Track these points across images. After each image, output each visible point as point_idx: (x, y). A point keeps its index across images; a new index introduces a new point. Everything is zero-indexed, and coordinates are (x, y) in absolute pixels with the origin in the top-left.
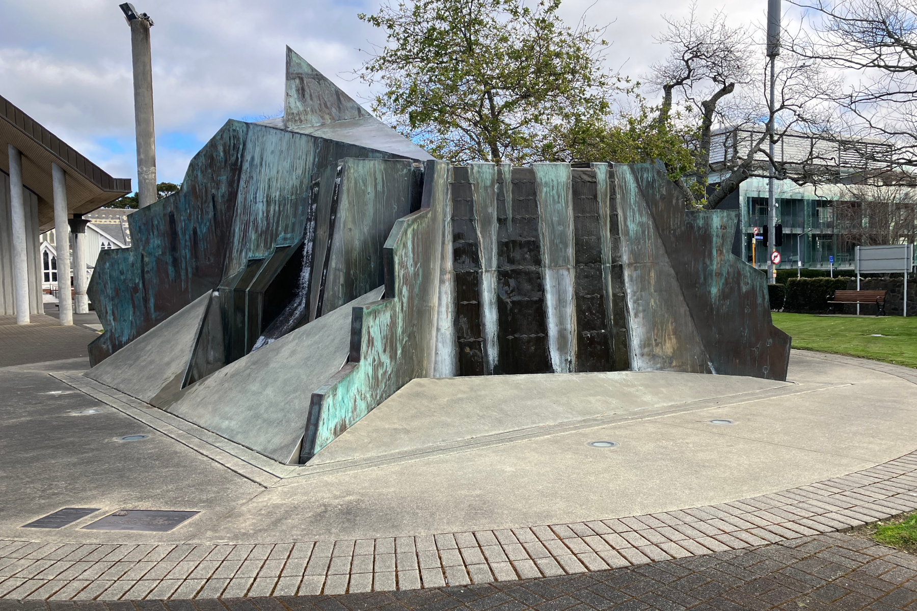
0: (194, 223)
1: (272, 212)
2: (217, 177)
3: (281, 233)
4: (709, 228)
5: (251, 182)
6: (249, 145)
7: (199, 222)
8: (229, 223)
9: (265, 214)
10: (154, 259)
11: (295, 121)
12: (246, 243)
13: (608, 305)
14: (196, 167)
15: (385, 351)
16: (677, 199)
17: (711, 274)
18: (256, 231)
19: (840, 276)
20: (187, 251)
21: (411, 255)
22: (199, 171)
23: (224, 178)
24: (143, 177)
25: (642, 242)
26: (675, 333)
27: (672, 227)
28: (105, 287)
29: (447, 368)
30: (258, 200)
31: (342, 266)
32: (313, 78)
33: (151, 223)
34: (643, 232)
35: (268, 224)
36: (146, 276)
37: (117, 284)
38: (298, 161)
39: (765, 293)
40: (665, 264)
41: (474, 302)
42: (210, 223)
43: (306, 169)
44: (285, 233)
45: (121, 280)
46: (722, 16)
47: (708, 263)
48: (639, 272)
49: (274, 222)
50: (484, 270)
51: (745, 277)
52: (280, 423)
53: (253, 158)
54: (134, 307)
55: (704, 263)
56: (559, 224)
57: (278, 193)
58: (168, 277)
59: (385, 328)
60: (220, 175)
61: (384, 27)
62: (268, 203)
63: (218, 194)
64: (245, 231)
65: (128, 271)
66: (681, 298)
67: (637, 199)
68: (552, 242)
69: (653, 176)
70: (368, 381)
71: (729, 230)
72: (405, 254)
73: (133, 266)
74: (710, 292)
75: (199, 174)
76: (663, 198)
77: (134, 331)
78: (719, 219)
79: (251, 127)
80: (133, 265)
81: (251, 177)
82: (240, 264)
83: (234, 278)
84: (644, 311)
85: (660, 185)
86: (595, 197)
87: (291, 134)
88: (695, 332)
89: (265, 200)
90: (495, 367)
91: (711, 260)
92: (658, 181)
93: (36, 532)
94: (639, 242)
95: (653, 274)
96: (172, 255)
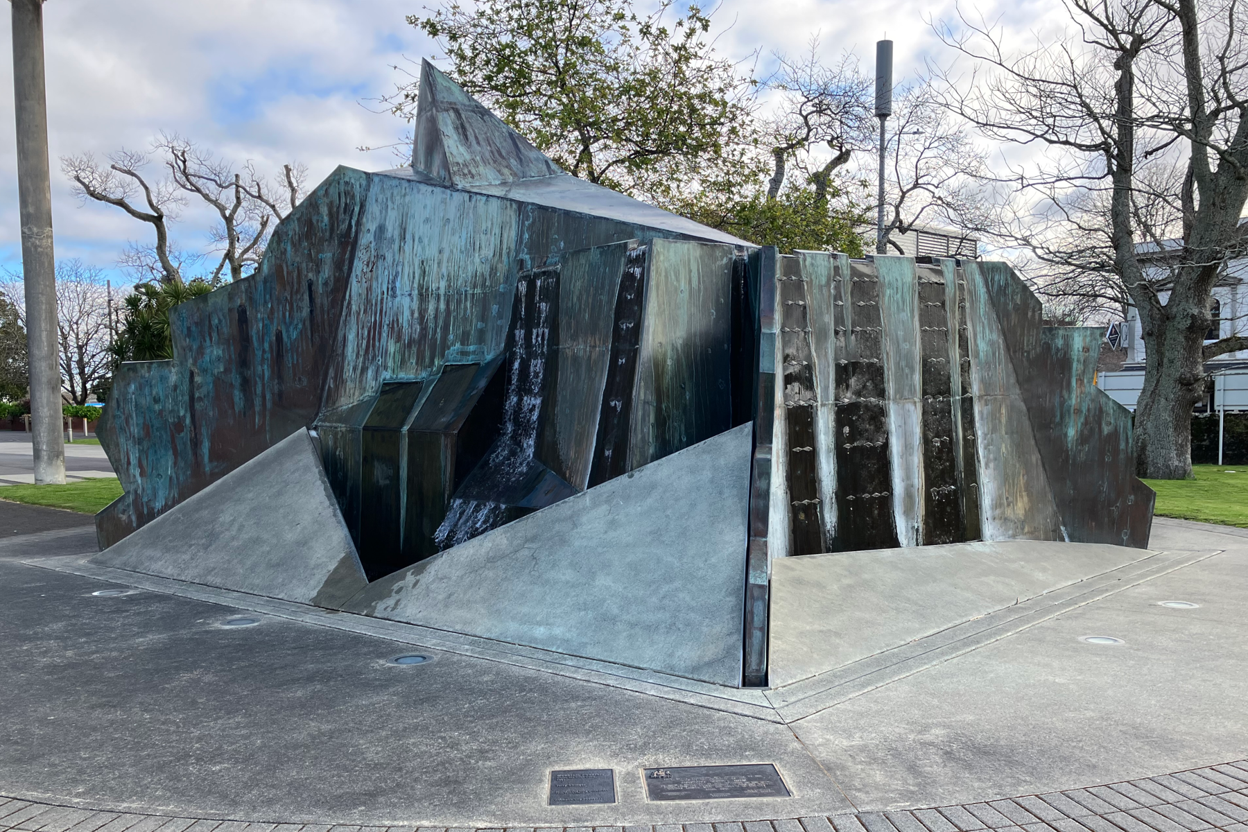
0: (278, 324)
2: (318, 253)
6: (373, 209)
7: (285, 323)
9: (416, 315)
10: (210, 379)
11: (465, 175)
12: (374, 357)
13: (958, 452)
17: (1069, 411)
18: (399, 339)
20: (266, 367)
22: (289, 244)
23: (327, 256)
24: (33, 244)
25: (992, 366)
26: (1027, 490)
27: (1026, 348)
28: (127, 422)
29: (779, 542)
30: (398, 292)
31: (651, 398)
32: (474, 112)
33: (207, 323)
34: (994, 354)
35: (424, 329)
36: (197, 406)
37: (147, 417)
38: (483, 237)
40: (1016, 394)
41: (808, 449)
42: (304, 324)
43: (501, 249)
45: (155, 412)
46: (853, 58)
47: (1066, 397)
48: (989, 407)
50: (819, 404)
51: (1108, 414)
52: (674, 628)
53: (381, 229)
54: (175, 453)
55: (1061, 396)
56: (905, 341)
57: (443, 284)
58: (233, 408)
60: (321, 251)
61: (444, 38)
62: (423, 295)
63: (318, 280)
65: (167, 397)
66: (1033, 442)
68: (897, 364)
71: (1092, 353)
74: (1066, 435)
75: (289, 248)
76: (1016, 308)
77: (175, 493)
78: (1081, 338)
79: (376, 179)
80: (175, 388)
84: (995, 459)
85: (1013, 291)
86: (943, 304)
87: (467, 196)
88: (1047, 489)
89: (415, 292)
90: (835, 540)
91: (1070, 392)
93: (600, 810)
94: (990, 367)
95: (1003, 411)
96: (241, 374)
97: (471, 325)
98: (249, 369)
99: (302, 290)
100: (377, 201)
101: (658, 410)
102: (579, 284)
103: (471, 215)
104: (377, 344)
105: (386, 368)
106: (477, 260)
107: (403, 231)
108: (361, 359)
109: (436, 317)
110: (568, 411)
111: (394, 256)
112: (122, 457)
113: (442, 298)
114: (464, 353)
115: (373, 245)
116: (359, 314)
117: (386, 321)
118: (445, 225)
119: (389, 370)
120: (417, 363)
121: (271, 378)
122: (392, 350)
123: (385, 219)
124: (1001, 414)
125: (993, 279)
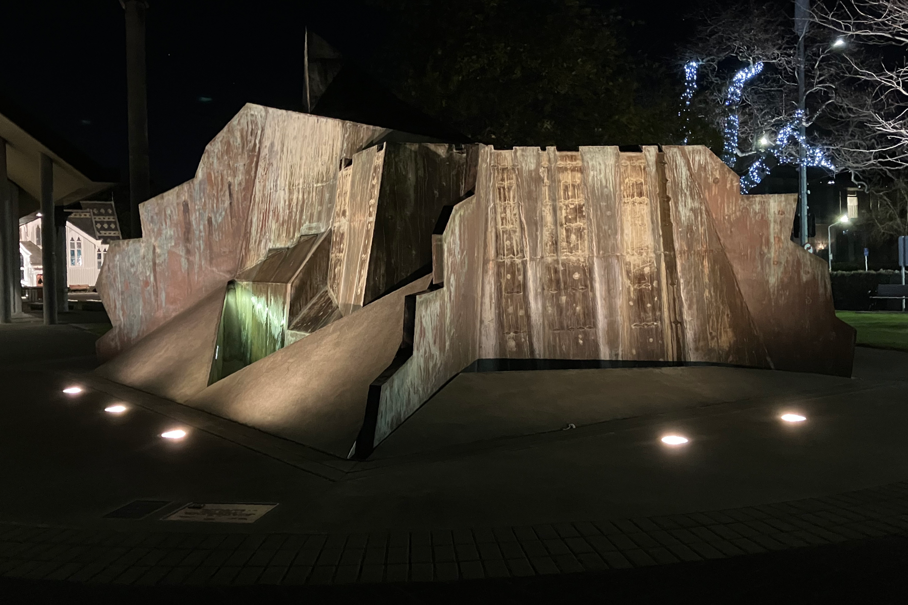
0: (209, 213)
1: (295, 201)
2: (234, 163)
3: (305, 222)
4: (766, 213)
5: (270, 169)
6: (268, 131)
7: (214, 212)
8: (247, 211)
9: (287, 203)
12: (265, 233)
14: (212, 154)
15: (435, 343)
16: (732, 183)
19: (881, 269)
20: (201, 242)
21: (459, 242)
22: (215, 158)
23: (241, 164)
30: (278, 188)
33: (163, 213)
34: (696, 218)
35: (290, 213)
36: (158, 269)
38: (323, 146)
39: (827, 283)
44: (310, 222)
45: (131, 273)
47: (766, 251)
49: (297, 211)
51: (805, 265)
53: (272, 145)
57: (301, 181)
59: (435, 318)
64: (265, 220)
65: (138, 263)
67: (689, 183)
69: (706, 159)
70: (420, 373)
72: (453, 240)
73: (144, 258)
74: (768, 282)
75: (215, 161)
76: (716, 181)
81: (271, 164)
82: (259, 256)
83: (252, 270)
85: (713, 168)
91: (769, 249)
92: (711, 163)
95: (706, 263)
96: (186, 247)
97: (315, 209)
98: (190, 243)
99: (224, 189)
101: (388, 265)
108: (259, 235)
112: (111, 303)
114: (310, 228)
115: (267, 156)
119: (272, 242)
120: (286, 237)
122: (274, 227)
124: (703, 266)
125: (694, 159)
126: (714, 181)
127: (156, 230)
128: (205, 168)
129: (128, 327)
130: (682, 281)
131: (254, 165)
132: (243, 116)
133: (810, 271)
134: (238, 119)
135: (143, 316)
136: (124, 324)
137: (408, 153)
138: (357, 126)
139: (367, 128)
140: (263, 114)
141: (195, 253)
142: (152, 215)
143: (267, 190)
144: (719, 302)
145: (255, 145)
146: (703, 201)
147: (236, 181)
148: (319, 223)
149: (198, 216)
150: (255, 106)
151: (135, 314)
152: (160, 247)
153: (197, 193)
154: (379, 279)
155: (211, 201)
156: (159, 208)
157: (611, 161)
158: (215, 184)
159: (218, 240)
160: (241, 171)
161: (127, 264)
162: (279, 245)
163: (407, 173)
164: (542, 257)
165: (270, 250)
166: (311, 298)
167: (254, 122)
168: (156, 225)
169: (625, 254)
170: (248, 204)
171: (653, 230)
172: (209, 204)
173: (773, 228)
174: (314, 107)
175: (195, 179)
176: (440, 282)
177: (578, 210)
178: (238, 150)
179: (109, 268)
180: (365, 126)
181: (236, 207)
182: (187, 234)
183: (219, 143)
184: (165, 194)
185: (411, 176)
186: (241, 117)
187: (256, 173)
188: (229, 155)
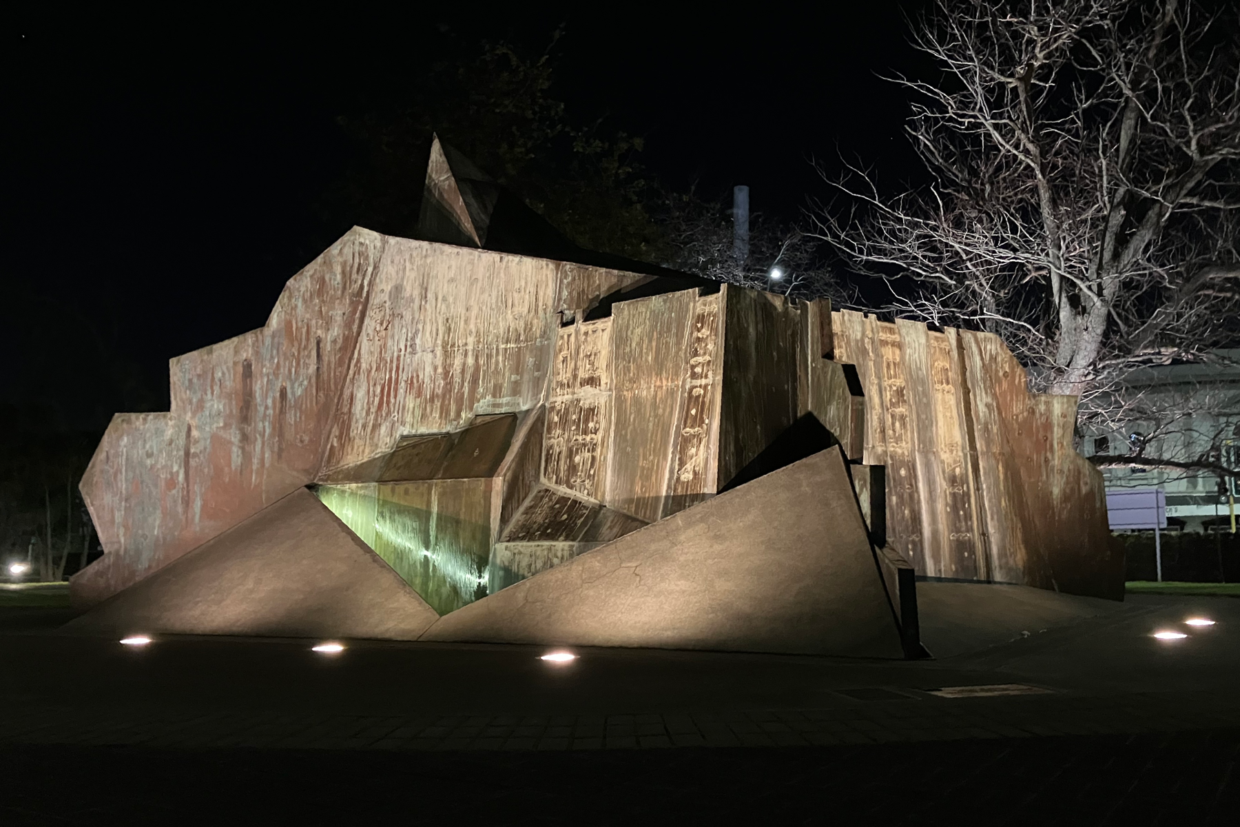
9: (440, 370)
14: (297, 293)
18: (419, 394)
20: (267, 424)
22: (300, 300)
23: (338, 313)
27: (1015, 412)
33: (210, 375)
35: (449, 385)
36: (193, 462)
37: (138, 472)
38: (516, 295)
42: (310, 380)
43: (537, 306)
45: (146, 467)
47: (1050, 458)
49: (463, 382)
51: (1085, 475)
53: (398, 289)
57: (471, 340)
60: (333, 308)
65: (161, 451)
71: (1069, 419)
74: (1051, 492)
75: (300, 304)
78: (1060, 405)
85: (1003, 360)
97: (504, 378)
98: (250, 425)
99: (310, 347)
100: (392, 262)
102: (638, 331)
103: (502, 275)
104: (392, 400)
105: (403, 423)
106: (510, 317)
107: (425, 290)
108: (372, 417)
109: (463, 371)
110: (629, 449)
111: (413, 314)
113: (470, 353)
116: (369, 372)
117: (403, 377)
118: (472, 284)
119: (408, 426)
120: (441, 417)
121: (272, 436)
122: (411, 406)
123: (403, 279)
125: (985, 348)
126: (1004, 375)
127: (194, 400)
128: (283, 313)
129: (132, 553)
130: (984, 486)
131: (358, 315)
132: (348, 244)
133: (1089, 481)
134: (339, 248)
135: (161, 535)
136: (125, 549)
137: (748, 300)
138: (587, 269)
139: (606, 272)
140: (379, 244)
141: (256, 439)
142: (191, 377)
143: (389, 352)
144: (1013, 514)
145: (362, 286)
146: (994, 396)
147: (329, 337)
148: (517, 397)
149: (265, 383)
150: (366, 231)
151: (147, 533)
152: (198, 428)
153: (267, 348)
154: (729, 458)
155: (287, 364)
156: (203, 366)
157: (923, 340)
158: (297, 339)
159: (293, 423)
160: (338, 323)
161: (140, 452)
162: (423, 430)
163: (748, 326)
164: (873, 447)
165: (403, 438)
166: (523, 500)
167: (363, 254)
168: (195, 392)
169: (939, 450)
170: (345, 371)
171: (960, 425)
172: (284, 367)
173: (1057, 432)
174: (484, 241)
175: (265, 329)
176: (859, 456)
177: (900, 392)
178: (335, 292)
179: (108, 458)
180: (603, 270)
181: (326, 375)
182: (245, 408)
183: (309, 279)
184: (215, 346)
185: (752, 330)
186: (345, 245)
187: (360, 327)
188: (321, 298)
